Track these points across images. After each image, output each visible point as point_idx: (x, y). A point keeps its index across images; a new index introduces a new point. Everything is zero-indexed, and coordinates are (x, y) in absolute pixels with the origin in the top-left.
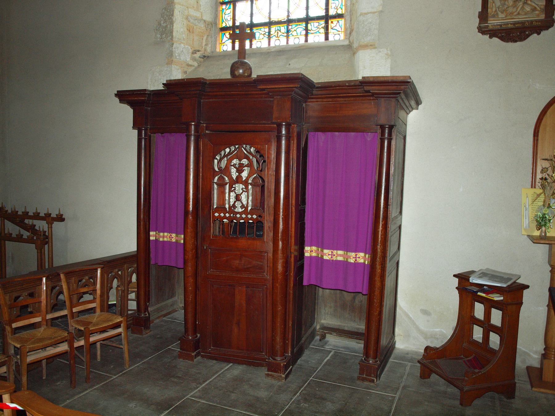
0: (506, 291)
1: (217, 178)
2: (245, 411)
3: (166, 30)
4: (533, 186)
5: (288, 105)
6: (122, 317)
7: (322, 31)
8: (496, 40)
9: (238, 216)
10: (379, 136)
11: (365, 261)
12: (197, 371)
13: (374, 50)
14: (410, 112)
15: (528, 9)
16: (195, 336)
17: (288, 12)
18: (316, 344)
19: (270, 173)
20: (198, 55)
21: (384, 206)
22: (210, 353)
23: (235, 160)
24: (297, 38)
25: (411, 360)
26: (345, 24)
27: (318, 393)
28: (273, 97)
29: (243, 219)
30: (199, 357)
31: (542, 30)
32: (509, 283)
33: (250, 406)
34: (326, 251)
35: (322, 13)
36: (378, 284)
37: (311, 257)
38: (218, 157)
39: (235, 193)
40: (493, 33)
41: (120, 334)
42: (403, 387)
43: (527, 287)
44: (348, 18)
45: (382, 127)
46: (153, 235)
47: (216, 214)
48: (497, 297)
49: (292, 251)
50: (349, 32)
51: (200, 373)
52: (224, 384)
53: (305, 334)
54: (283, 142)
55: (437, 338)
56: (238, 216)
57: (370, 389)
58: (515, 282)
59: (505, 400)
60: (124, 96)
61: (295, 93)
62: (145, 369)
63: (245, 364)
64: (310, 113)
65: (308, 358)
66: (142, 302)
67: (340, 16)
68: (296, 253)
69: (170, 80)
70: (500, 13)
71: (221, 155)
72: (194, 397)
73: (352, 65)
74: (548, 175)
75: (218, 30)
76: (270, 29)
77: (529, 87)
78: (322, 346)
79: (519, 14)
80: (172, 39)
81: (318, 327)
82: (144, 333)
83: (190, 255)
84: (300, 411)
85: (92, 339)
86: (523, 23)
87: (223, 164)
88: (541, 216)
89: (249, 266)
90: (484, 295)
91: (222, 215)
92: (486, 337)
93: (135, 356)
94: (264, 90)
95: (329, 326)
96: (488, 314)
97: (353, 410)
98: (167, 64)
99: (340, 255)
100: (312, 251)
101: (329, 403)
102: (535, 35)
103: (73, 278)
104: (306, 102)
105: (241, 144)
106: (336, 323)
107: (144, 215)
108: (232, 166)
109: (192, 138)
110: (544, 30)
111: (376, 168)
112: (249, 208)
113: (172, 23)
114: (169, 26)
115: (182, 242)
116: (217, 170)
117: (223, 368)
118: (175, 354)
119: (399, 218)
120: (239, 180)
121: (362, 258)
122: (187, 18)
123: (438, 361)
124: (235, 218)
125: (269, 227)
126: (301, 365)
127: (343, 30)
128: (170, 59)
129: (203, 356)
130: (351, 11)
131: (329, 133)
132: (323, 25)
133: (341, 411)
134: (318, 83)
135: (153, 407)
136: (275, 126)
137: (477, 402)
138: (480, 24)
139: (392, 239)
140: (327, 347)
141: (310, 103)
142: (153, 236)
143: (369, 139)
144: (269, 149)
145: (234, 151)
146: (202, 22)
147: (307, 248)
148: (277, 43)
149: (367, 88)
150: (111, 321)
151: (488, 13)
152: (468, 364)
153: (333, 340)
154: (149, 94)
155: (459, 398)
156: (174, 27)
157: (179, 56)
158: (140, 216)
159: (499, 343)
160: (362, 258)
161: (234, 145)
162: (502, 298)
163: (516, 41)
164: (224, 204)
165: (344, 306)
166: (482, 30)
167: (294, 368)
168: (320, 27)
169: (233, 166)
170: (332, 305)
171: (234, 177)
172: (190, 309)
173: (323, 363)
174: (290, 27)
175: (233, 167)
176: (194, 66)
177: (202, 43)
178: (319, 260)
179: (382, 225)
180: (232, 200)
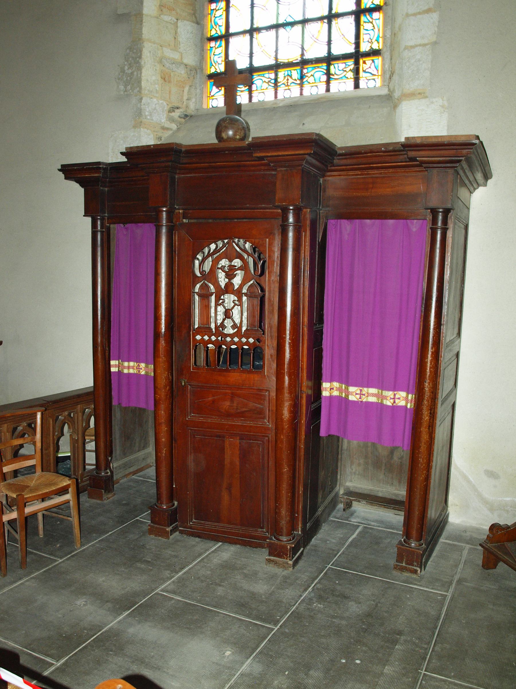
1: (198, 286)
2: (236, 613)
3: (131, 78)
5: (297, 181)
6: (69, 480)
7: (351, 75)
9: (228, 339)
10: (430, 225)
11: (407, 403)
12: (173, 553)
13: (423, 101)
14: (475, 189)
16: (171, 504)
17: (303, 49)
18: (338, 515)
19: (272, 278)
20: (176, 114)
21: (434, 325)
22: (191, 528)
23: (224, 260)
24: (315, 86)
25: (470, 541)
26: (383, 65)
27: (339, 588)
28: (275, 170)
29: (235, 343)
30: (177, 533)
33: (242, 606)
34: (352, 389)
35: (351, 49)
36: (425, 437)
37: (331, 397)
38: (200, 257)
39: (224, 307)
41: (68, 502)
42: (458, 581)
44: (387, 55)
45: (434, 212)
46: (114, 365)
47: (198, 337)
49: (304, 389)
50: (388, 76)
51: (176, 557)
52: (209, 572)
53: (322, 503)
54: (291, 234)
56: (228, 339)
57: (412, 583)
60: (70, 172)
61: (307, 162)
62: (102, 549)
63: (239, 544)
64: (330, 192)
65: (326, 536)
66: (102, 457)
67: (375, 53)
68: (310, 392)
69: (131, 148)
71: (204, 253)
72: (167, 591)
73: (391, 123)
75: (205, 78)
76: (276, 75)
78: (347, 519)
80: (140, 92)
81: (342, 492)
82: (105, 497)
83: (163, 394)
84: (312, 614)
85: (28, 510)
87: (208, 266)
89: (244, 409)
91: (206, 338)
93: (87, 532)
94: (262, 158)
95: (357, 491)
97: (386, 614)
98: (135, 127)
99: (373, 395)
100: (333, 389)
101: (353, 603)
103: (6, 425)
104: (324, 176)
105: (231, 238)
106: (366, 487)
107: (102, 337)
108: (219, 268)
109: (164, 230)
111: (424, 272)
112: (244, 329)
113: (140, 69)
114: (135, 73)
115: (152, 374)
116: (198, 274)
117: (208, 550)
118: (146, 528)
119: (457, 342)
120: (229, 289)
121: (403, 399)
122: (160, 62)
123: (508, 545)
124: (225, 342)
125: (271, 356)
126: (315, 546)
127: (380, 73)
128: (138, 120)
129: (181, 532)
130: (391, 45)
131: (357, 220)
132: (352, 67)
133: (369, 615)
134: (342, 148)
135: (109, 605)
136: (280, 211)
139: (446, 372)
140: (354, 520)
141: (330, 178)
142: (115, 366)
143: (414, 230)
144: (270, 244)
145: (221, 248)
146: (183, 66)
147: (325, 385)
148: (287, 94)
149: (412, 154)
150: (55, 484)
153: (362, 510)
154: (104, 169)
156: (143, 75)
157: (151, 115)
158: (97, 340)
160: (403, 399)
161: (222, 239)
164: (209, 322)
165: (377, 464)
167: (306, 551)
168: (348, 70)
169: (221, 268)
170: (362, 461)
171: (223, 284)
172: (164, 469)
173: (347, 544)
174: (305, 71)
175: (220, 271)
176: (171, 129)
177: (182, 96)
178: (343, 402)
179: (432, 353)
180: (220, 317)
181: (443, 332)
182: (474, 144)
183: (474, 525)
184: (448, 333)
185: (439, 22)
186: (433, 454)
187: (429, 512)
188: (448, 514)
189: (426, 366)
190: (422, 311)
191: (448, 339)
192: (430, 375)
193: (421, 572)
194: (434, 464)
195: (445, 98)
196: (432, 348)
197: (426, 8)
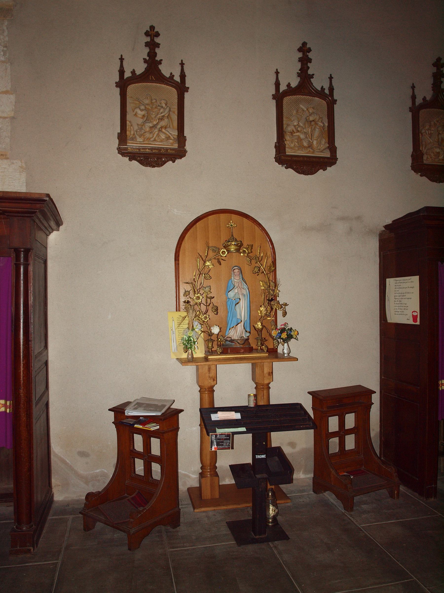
0: (161, 420)
4: (178, 309)
8: (135, 163)
10: (14, 261)
13: (5, 161)
14: (50, 233)
15: (163, 136)
31: (176, 159)
32: (163, 411)
40: (132, 156)
43: (182, 411)
48: (153, 427)
55: (99, 480)
58: (169, 408)
59: (171, 530)
70: (138, 137)
74: (191, 298)
77: (168, 212)
79: (155, 140)
86: (159, 149)
88: (187, 339)
90: (140, 427)
92: (148, 469)
96: (147, 445)
102: (171, 162)
110: (178, 159)
119: (45, 353)
137: (146, 541)
138: (119, 145)
139: (38, 379)
151: (127, 135)
152: (132, 502)
155: (127, 542)
159: (160, 471)
162: (158, 427)
163: (154, 167)
166: (122, 152)
181: (31, 347)
182: (45, 201)
183: (75, 498)
184: (36, 348)
185: (16, 102)
186: (33, 447)
187: (35, 498)
188: (53, 494)
189: (20, 376)
190: (12, 331)
191: (36, 352)
192: (23, 382)
193: (34, 550)
194: (35, 455)
195: (23, 161)
196: (23, 361)
197: (4, 90)
